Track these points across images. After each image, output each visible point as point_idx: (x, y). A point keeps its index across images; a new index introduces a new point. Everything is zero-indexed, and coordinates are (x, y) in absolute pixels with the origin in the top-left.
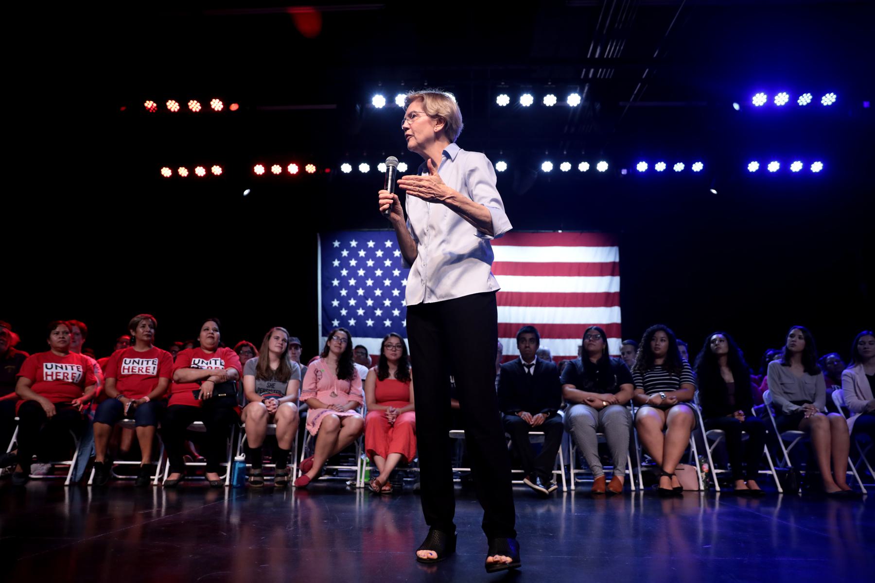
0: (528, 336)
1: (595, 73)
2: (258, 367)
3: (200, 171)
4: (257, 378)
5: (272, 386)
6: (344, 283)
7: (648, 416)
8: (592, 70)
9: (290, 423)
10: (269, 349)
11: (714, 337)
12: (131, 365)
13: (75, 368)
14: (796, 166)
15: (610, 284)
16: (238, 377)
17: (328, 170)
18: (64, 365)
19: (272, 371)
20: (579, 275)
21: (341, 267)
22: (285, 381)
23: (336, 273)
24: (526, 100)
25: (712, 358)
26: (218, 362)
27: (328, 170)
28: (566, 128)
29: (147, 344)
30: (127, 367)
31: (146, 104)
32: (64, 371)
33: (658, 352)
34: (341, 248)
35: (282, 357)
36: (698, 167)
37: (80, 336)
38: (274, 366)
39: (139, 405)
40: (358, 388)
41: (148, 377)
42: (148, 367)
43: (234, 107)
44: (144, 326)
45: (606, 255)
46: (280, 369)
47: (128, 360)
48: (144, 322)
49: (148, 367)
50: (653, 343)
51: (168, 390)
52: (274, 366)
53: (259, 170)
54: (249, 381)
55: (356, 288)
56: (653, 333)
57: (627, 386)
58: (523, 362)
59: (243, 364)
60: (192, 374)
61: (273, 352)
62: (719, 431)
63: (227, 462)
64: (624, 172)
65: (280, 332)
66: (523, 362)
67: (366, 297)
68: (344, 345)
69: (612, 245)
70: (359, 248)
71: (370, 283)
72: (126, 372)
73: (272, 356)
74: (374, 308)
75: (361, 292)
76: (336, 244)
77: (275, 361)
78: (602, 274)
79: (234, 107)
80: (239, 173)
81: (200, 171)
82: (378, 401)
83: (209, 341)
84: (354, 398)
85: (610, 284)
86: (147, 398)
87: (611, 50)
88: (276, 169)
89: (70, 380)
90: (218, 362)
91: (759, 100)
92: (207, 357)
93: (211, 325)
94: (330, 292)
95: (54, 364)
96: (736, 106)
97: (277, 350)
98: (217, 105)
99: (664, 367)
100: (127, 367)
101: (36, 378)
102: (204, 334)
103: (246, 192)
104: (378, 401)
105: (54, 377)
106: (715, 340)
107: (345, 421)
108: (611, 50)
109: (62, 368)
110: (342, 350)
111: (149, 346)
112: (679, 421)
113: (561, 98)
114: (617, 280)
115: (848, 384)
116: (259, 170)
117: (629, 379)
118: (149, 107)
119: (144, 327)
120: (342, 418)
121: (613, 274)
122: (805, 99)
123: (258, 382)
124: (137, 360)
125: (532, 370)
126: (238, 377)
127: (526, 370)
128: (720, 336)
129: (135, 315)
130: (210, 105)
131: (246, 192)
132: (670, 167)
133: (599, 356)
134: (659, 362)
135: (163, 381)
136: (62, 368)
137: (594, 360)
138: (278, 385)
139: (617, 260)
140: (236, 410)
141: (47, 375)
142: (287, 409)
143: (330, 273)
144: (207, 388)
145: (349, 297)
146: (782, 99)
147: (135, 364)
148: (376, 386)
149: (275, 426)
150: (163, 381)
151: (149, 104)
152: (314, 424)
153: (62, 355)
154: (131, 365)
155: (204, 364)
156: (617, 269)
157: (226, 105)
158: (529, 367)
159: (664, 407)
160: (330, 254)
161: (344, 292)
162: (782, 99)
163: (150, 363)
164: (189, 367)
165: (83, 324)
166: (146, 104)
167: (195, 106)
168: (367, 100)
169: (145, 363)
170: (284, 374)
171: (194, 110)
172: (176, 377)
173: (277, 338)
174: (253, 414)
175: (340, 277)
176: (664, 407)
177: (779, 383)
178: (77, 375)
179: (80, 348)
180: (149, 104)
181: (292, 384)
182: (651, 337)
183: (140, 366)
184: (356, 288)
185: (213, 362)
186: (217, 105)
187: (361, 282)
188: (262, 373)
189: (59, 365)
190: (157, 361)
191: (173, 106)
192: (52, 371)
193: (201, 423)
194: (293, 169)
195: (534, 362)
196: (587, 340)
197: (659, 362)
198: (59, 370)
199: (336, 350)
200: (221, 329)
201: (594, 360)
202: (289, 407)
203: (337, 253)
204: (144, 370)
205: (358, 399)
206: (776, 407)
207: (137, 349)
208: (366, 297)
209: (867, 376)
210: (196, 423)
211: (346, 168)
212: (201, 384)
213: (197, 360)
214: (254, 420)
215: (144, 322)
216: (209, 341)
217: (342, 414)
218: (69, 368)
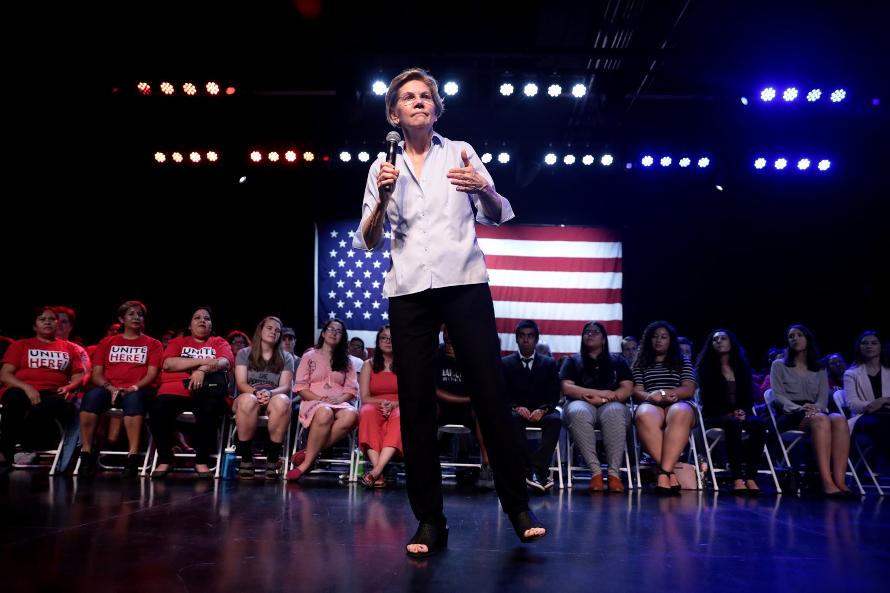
0: (527, 331)
1: (602, 64)
2: (251, 357)
3: (195, 157)
4: (249, 368)
5: (265, 376)
6: (341, 274)
7: (647, 413)
8: (599, 61)
9: (282, 415)
10: (261, 339)
11: (717, 334)
12: (119, 353)
13: (61, 355)
14: (804, 164)
15: (612, 280)
16: (229, 367)
17: (326, 159)
18: (50, 352)
19: (265, 361)
20: (581, 270)
21: (338, 258)
22: (278, 372)
23: (333, 264)
24: (781, 164)
25: (714, 356)
26: (209, 352)
27: (326, 159)
28: (571, 120)
29: (136, 332)
30: (115, 354)
31: (139, 86)
32: (129, 354)
33: (659, 349)
34: (339, 239)
35: (275, 347)
36: (704, 162)
37: (68, 324)
38: (267, 356)
39: (128, 394)
40: (353, 380)
41: (137, 366)
42: (137, 355)
43: (230, 91)
44: (132, 314)
45: (609, 250)
46: (273, 359)
47: (116, 348)
48: (133, 310)
49: (137, 355)
50: (654, 340)
51: (157, 379)
52: (267, 356)
53: (256, 156)
54: (241, 371)
55: (354, 279)
56: (654, 329)
57: (626, 383)
58: (521, 357)
59: (235, 355)
60: (182, 363)
61: (266, 342)
62: (719, 430)
63: (217, 453)
64: (629, 166)
65: (273, 321)
66: (521, 357)
67: (363, 289)
68: (338, 336)
69: (615, 240)
70: (373, 259)
71: (367, 274)
72: (114, 360)
73: (265, 346)
74: (372, 300)
75: (358, 284)
76: (334, 234)
77: (267, 351)
78: (604, 270)
79: (230, 91)
80: (235, 159)
81: (195, 157)
82: (373, 394)
83: (201, 329)
84: (347, 390)
85: (612, 280)
86: (135, 387)
87: (618, 41)
88: (274, 157)
89: (56, 368)
90: (209, 352)
91: (768, 94)
92: (198, 346)
93: (202, 313)
94: (327, 284)
95: (39, 351)
96: (744, 101)
97: (270, 340)
98: (213, 88)
99: (665, 364)
100: (115, 354)
101: (21, 365)
102: (195, 322)
103: (242, 179)
104: (373, 394)
105: (40, 364)
106: (717, 337)
107: (339, 414)
108: (618, 41)
109: (47, 355)
110: (337, 341)
111: (138, 334)
112: (679, 418)
113: (567, 89)
114: (619, 276)
115: (849, 385)
116: (256, 156)
117: (629, 376)
118: (143, 88)
119: (133, 315)
120: (335, 411)
121: (615, 270)
122: (814, 95)
123: (250, 373)
124: (125, 347)
125: (530, 365)
126: (229, 367)
127: (525, 364)
128: (723, 333)
129: (124, 302)
130: (206, 89)
131: (242, 179)
132: (675, 162)
133: (599, 351)
134: (660, 359)
135: (152, 370)
136: (47, 355)
137: (594, 356)
138: (271, 376)
139: (620, 256)
140: (228, 400)
141: (32, 362)
142: (280, 400)
143: (327, 264)
144: (197, 378)
145: (346, 289)
146: (791, 94)
147: (124, 352)
148: (371, 379)
149: (266, 417)
150: (152, 370)
151: (143, 86)
152: (306, 416)
153: (48, 341)
154: (119, 353)
155: (195, 353)
156: (620, 265)
157: (223, 88)
158: (527, 362)
159: (664, 405)
160: (327, 244)
161: (341, 284)
162: (791, 94)
163: (139, 351)
164: (180, 356)
165: (71, 311)
166: (139, 86)
167: (190, 89)
168: (367, 87)
169: (134, 351)
170: (276, 365)
171: (189, 93)
172: (165, 366)
173: (271, 328)
174: (244, 406)
175: (337, 268)
176: (664, 405)
177: (782, 382)
178: (63, 363)
179: (67, 336)
180: (143, 86)
181: (285, 375)
182: (652, 334)
183: (129, 354)
184: (354, 279)
185: (204, 351)
186: (213, 88)
187: (359, 274)
188: (255, 363)
189: (45, 352)
190: (146, 349)
191: (167, 88)
192: (37, 357)
193: (191, 413)
194: (291, 156)
195: (533, 357)
196: (586, 336)
197: (660, 359)
198: (45, 357)
199: (331, 341)
200: (213, 318)
201: (594, 356)
202: (281, 399)
203: (334, 244)
204: (133, 358)
205: (352, 392)
206: (778, 407)
207: (126, 336)
208: (363, 289)
209: (870, 376)
210: (185, 413)
211: (345, 157)
212: (191, 374)
213: (187, 349)
214: (244, 412)
215: (133, 310)
216: (201, 329)
217: (336, 407)
218: (55, 355)
